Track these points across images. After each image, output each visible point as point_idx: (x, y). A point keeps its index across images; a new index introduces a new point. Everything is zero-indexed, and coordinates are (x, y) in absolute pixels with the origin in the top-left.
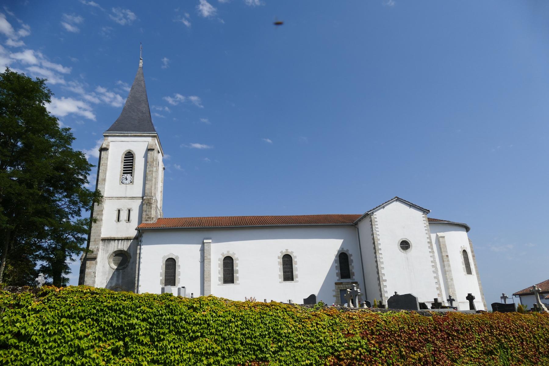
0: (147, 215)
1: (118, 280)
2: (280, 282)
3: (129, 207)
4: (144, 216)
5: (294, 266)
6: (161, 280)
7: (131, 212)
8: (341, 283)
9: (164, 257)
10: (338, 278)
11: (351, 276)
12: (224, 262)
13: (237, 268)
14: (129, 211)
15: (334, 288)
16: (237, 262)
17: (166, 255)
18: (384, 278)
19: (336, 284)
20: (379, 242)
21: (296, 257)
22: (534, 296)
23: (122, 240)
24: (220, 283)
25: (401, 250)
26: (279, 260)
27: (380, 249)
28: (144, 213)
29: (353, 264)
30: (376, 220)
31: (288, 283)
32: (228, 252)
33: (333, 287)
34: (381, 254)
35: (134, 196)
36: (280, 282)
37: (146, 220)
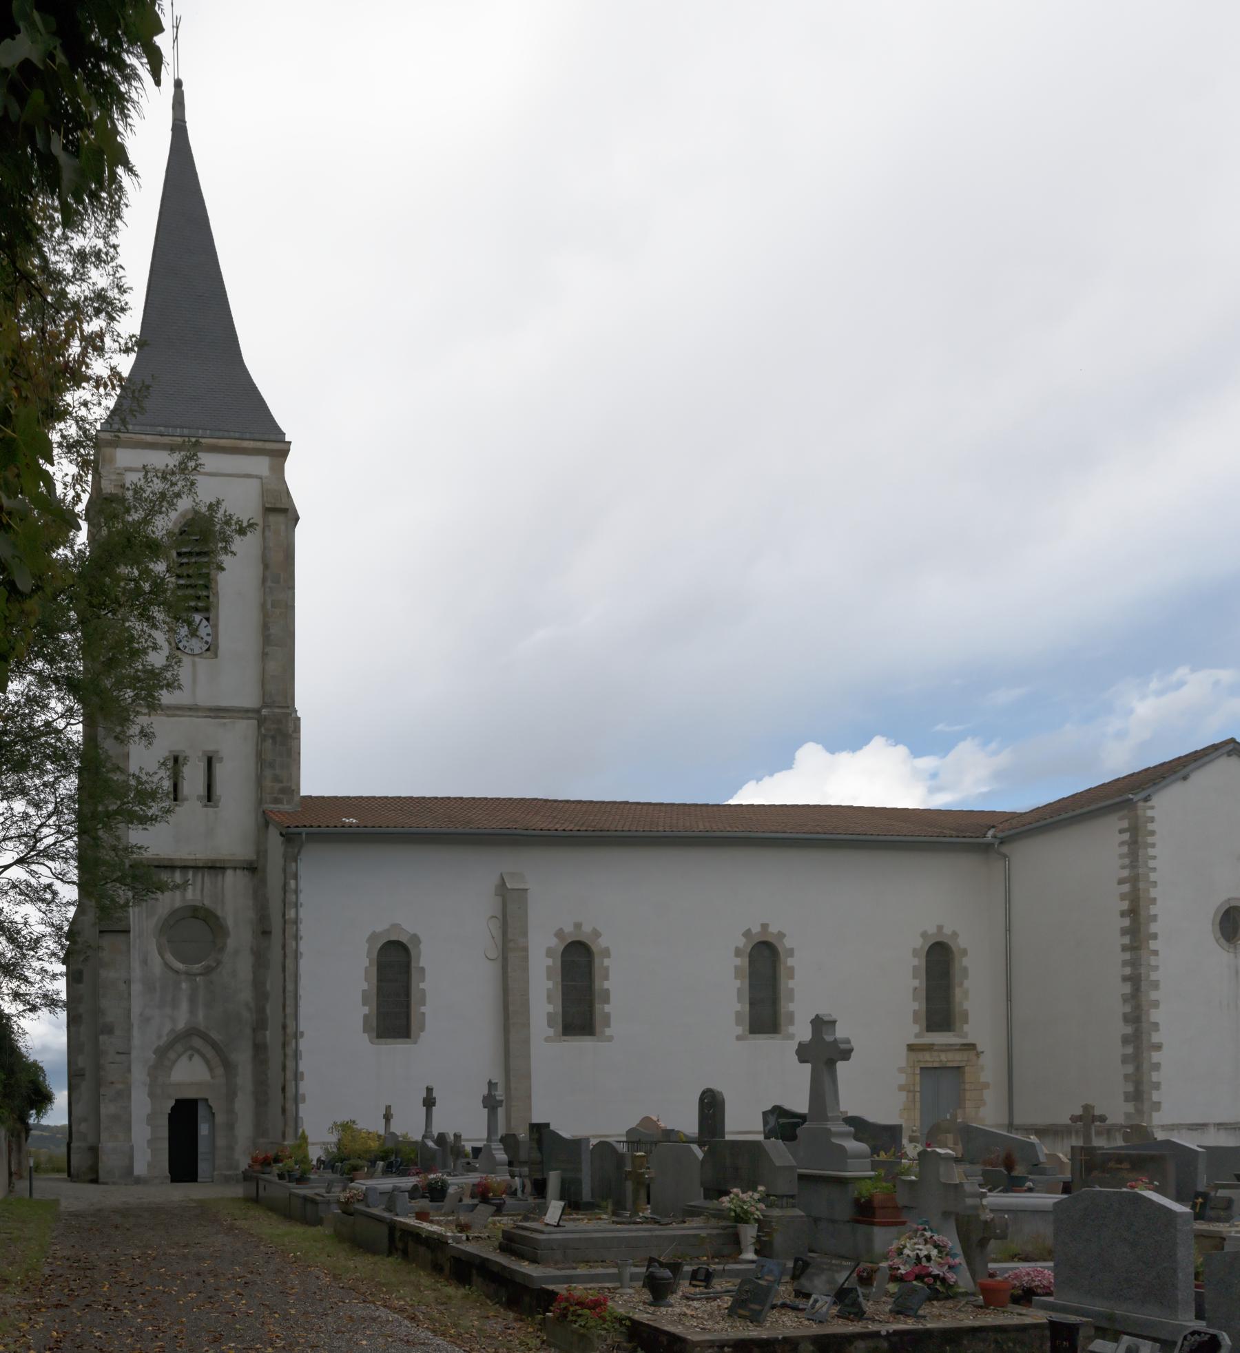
0: (277, 779)
1: (193, 1011)
2: (739, 1038)
3: (211, 747)
4: (268, 783)
5: (417, 985)
6: (366, 1017)
7: (219, 769)
8: (929, 1048)
9: (373, 937)
10: (916, 1029)
11: (598, 1029)
12: (563, 962)
13: (606, 985)
14: (210, 762)
15: (903, 1064)
16: (606, 962)
17: (379, 929)
18: (1155, 1038)
19: (911, 1048)
20: (1153, 910)
21: (791, 952)
22: (485, 1136)
23: (196, 868)
24: (551, 1032)
25: (1222, 940)
26: (738, 961)
27: (1155, 936)
28: (268, 773)
29: (966, 983)
30: (1150, 827)
31: (582, 1044)
32: (578, 926)
33: (901, 1058)
34: (1156, 953)
35: (224, 703)
36: (739, 1038)
37: (276, 801)
